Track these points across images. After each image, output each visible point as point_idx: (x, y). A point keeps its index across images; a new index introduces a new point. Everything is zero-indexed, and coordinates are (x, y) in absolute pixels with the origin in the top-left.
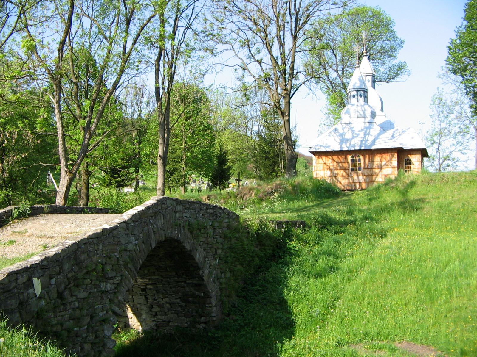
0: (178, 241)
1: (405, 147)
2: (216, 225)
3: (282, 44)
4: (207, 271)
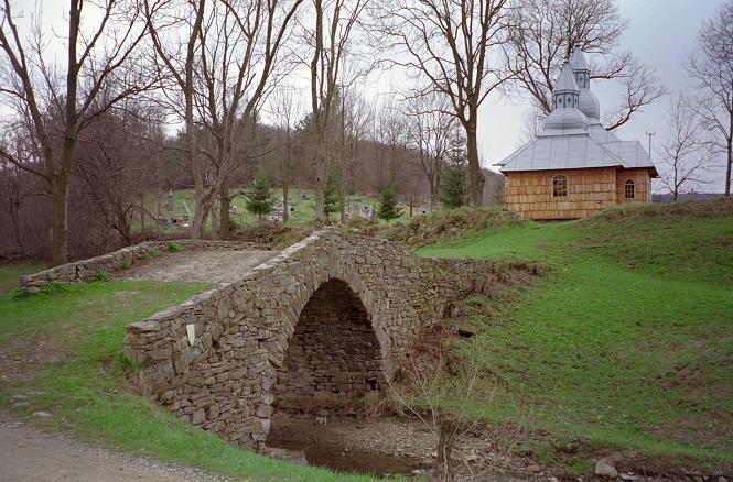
0: (345, 284)
1: (625, 166)
2: (387, 263)
3: (468, 36)
4: (375, 318)
